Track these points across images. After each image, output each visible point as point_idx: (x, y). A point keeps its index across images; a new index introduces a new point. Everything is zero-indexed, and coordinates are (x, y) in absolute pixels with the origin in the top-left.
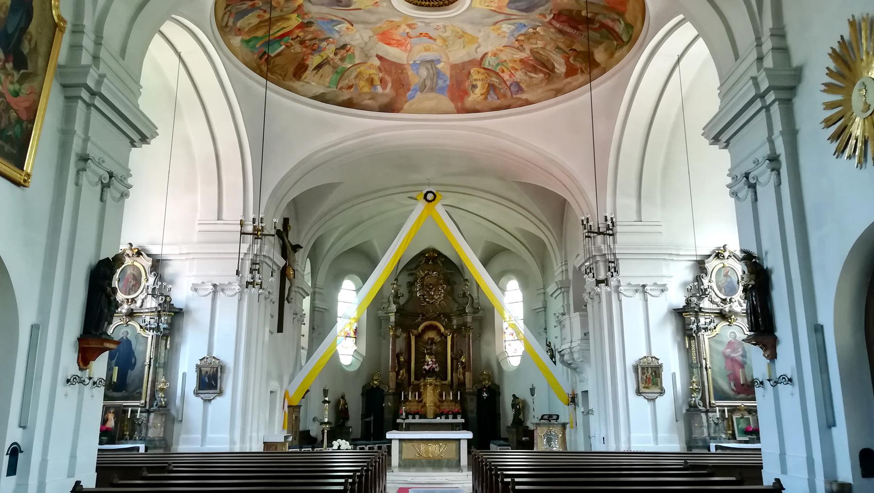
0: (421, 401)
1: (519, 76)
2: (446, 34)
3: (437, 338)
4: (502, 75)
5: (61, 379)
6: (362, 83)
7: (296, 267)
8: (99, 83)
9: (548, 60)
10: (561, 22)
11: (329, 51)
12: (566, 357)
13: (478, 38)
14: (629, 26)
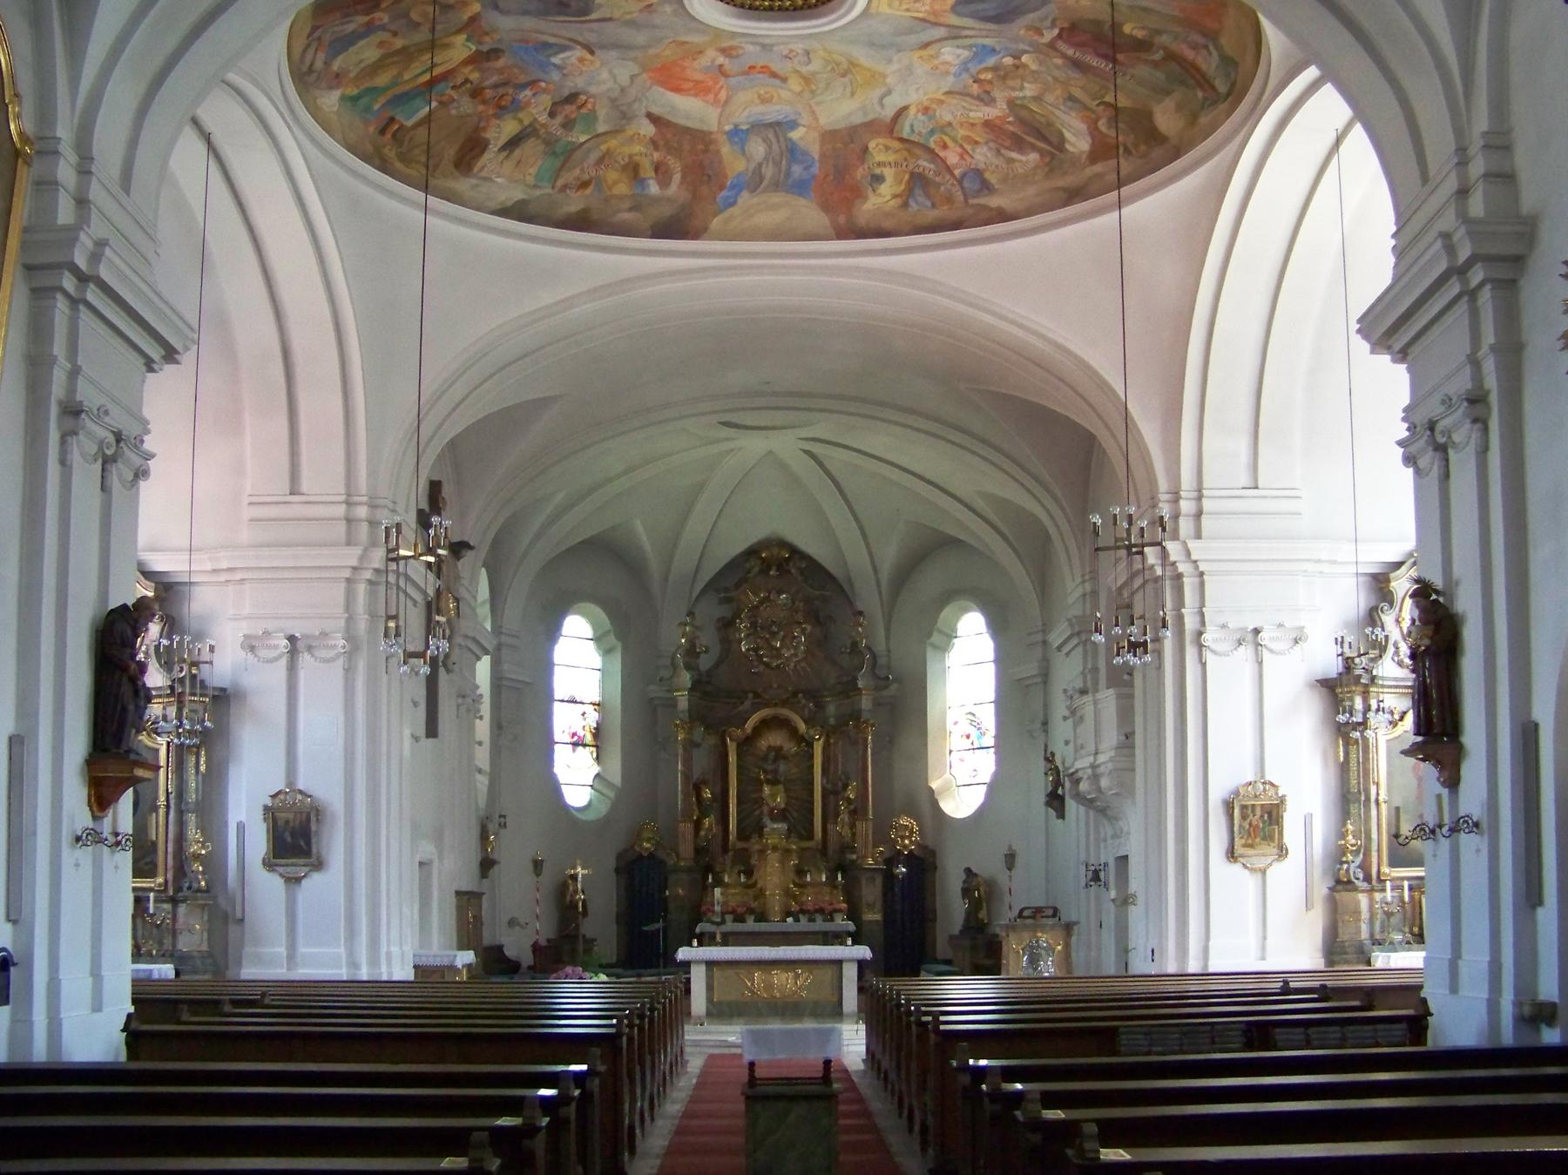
0: (755, 884)
1: (982, 156)
2: (811, 68)
3: (791, 747)
4: (942, 154)
5: (66, 838)
6: (612, 175)
7: (463, 593)
8: (95, 257)
9: (1050, 125)
10: (1079, 45)
11: (537, 108)
12: (1084, 786)
13: (884, 76)
14: (1228, 63)
